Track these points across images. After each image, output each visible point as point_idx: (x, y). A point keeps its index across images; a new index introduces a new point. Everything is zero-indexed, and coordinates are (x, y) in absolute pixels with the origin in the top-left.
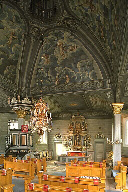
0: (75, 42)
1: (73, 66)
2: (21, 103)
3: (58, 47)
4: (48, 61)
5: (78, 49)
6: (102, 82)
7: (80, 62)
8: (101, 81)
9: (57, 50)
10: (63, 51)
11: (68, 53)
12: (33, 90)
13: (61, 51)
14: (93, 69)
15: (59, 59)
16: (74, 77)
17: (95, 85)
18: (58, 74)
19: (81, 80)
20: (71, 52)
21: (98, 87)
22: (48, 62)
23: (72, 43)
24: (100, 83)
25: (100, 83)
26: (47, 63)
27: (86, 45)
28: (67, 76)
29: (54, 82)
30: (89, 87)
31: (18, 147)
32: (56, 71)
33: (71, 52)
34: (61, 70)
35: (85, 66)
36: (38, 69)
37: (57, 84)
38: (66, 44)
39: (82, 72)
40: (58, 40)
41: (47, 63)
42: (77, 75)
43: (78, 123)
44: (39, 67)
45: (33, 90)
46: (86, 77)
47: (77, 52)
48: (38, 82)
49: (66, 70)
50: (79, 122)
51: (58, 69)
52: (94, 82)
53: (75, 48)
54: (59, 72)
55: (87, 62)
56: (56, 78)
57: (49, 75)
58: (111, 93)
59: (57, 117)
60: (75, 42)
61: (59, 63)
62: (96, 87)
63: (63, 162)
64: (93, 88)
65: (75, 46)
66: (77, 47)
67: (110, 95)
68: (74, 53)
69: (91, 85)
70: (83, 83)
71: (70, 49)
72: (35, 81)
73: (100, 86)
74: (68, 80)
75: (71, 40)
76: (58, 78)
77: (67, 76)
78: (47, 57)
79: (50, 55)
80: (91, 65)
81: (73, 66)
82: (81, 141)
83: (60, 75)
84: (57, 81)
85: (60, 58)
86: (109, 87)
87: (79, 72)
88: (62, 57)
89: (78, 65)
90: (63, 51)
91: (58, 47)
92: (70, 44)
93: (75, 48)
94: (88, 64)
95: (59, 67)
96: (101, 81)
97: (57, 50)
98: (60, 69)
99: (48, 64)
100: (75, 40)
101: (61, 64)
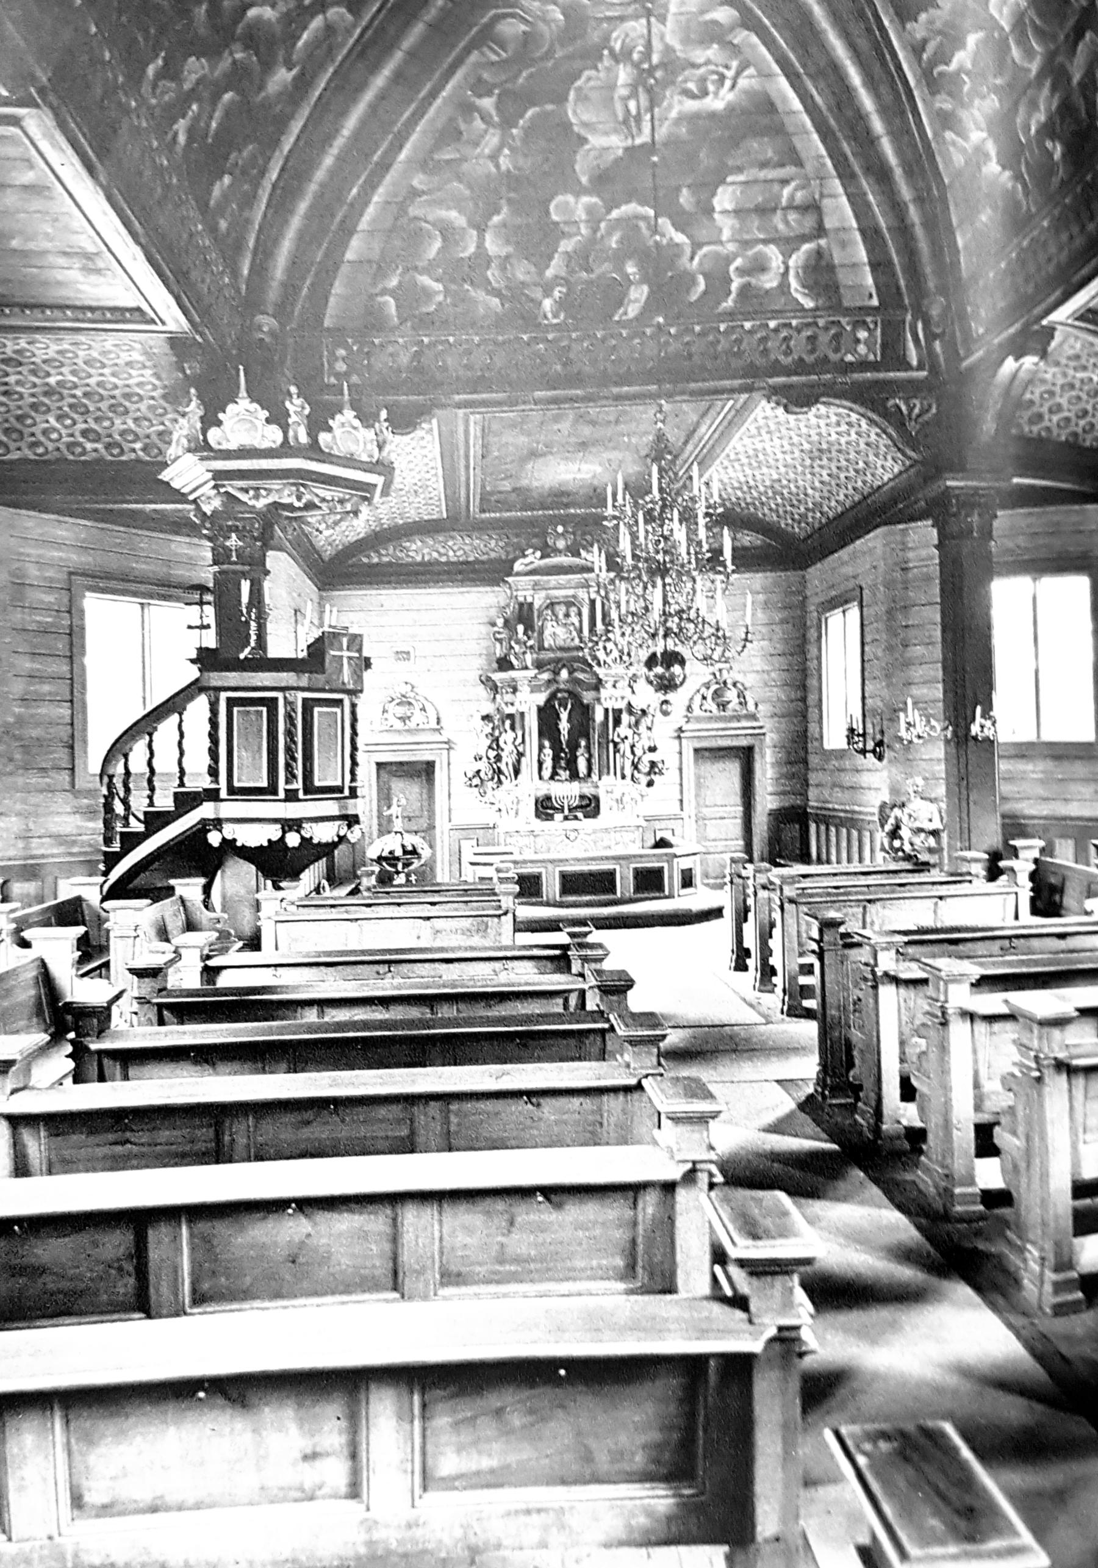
0: (735, 50)
1: (685, 198)
2: (314, 450)
3: (607, 62)
4: (511, 149)
5: (746, 92)
6: (876, 323)
7: (741, 178)
8: (869, 319)
9: (598, 79)
10: (634, 94)
11: (670, 107)
12: (348, 348)
13: (624, 92)
14: (820, 231)
15: (596, 141)
16: (687, 280)
17: (824, 338)
18: (566, 246)
19: (729, 303)
20: (691, 105)
21: (849, 358)
22: (506, 151)
23: (713, 52)
24: (862, 334)
25: (862, 334)
26: (494, 157)
27: (805, 77)
28: (631, 269)
29: (532, 300)
30: (788, 352)
31: (291, 796)
32: (557, 224)
33: (691, 105)
34: (594, 220)
35: (764, 211)
36: (415, 193)
37: (555, 316)
38: (668, 50)
39: (746, 244)
40: (622, 19)
41: (494, 157)
42: (707, 267)
43: (561, 610)
44: (418, 181)
45: (348, 348)
46: (769, 282)
47: (731, 109)
48: (392, 293)
49: (629, 224)
50: (569, 604)
51: (573, 207)
52: (821, 322)
53: (728, 83)
54: (574, 230)
55: (785, 182)
56: (549, 273)
57: (493, 246)
58: (930, 406)
59: (386, 559)
60: (735, 50)
61: (583, 168)
62: (834, 357)
63: (833, 858)
64: (809, 359)
65: (730, 74)
66: (742, 83)
67: (919, 416)
68: (713, 115)
69: (799, 343)
70: (748, 325)
71: (692, 86)
72: (374, 284)
73: (862, 349)
74: (639, 294)
75: (714, 34)
76: (563, 274)
77: (631, 269)
78: (508, 123)
79: (537, 109)
80: (813, 208)
81: (685, 198)
82: (588, 748)
83: (582, 258)
84: (557, 294)
85: (606, 134)
86: (915, 363)
87: (721, 243)
88: (616, 131)
89: (724, 199)
90: (634, 94)
91: (607, 62)
92: (700, 55)
93: (728, 83)
94: (792, 197)
95: (585, 199)
96: (869, 319)
97: (592, 83)
98: (590, 210)
99: (497, 166)
100: (742, 36)
101: (602, 180)
